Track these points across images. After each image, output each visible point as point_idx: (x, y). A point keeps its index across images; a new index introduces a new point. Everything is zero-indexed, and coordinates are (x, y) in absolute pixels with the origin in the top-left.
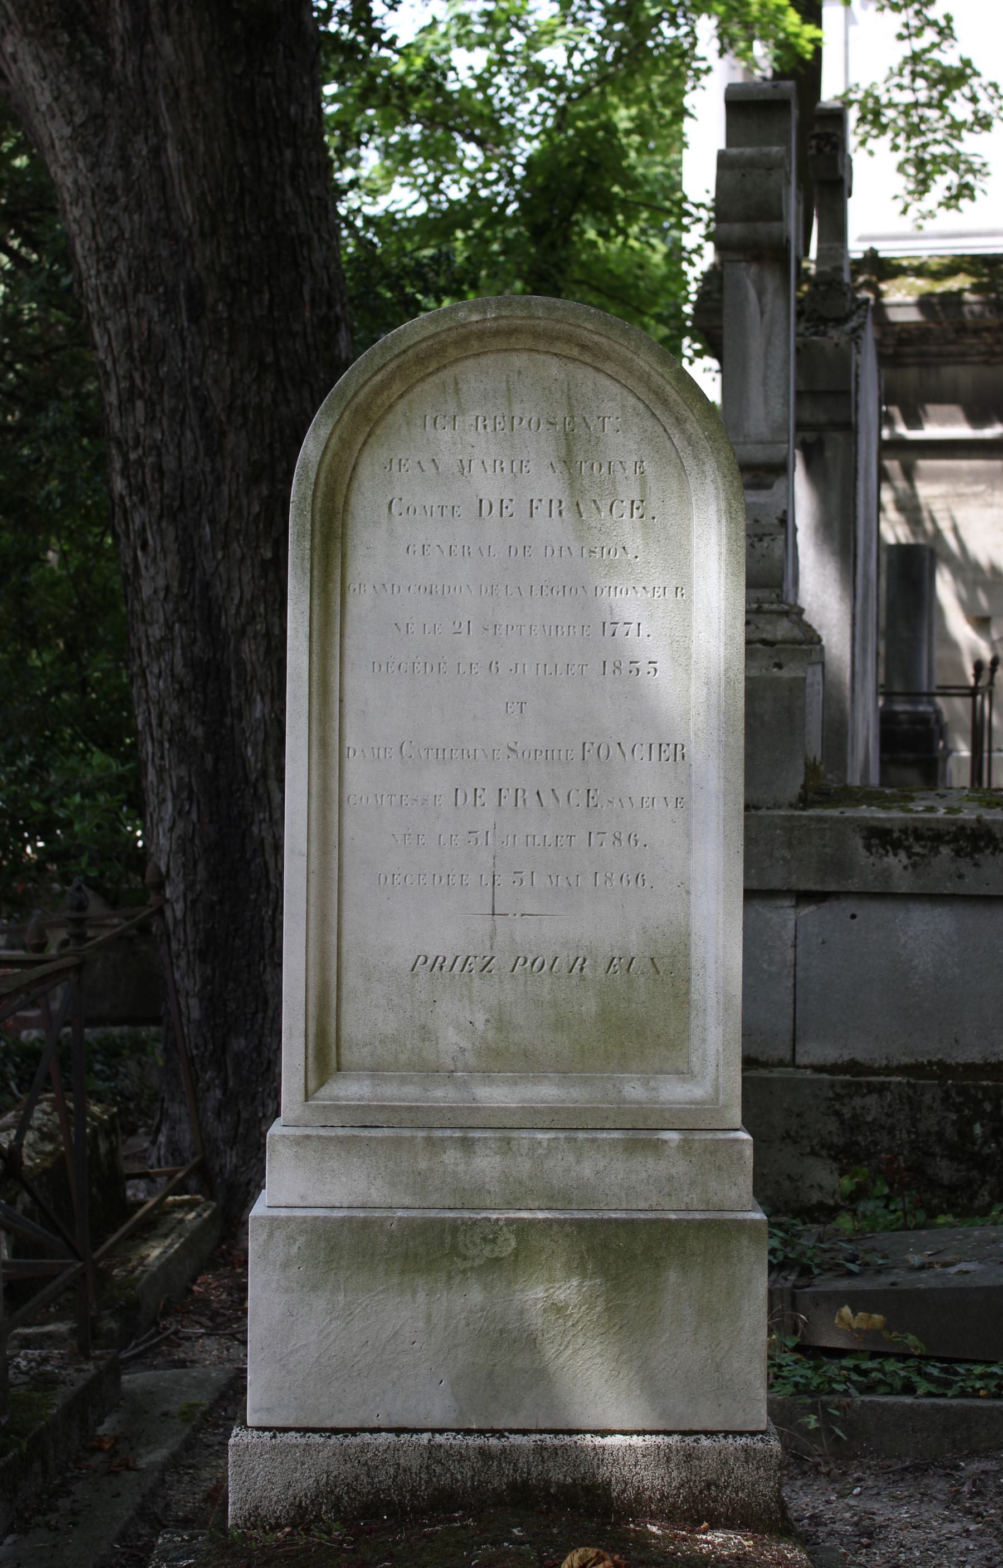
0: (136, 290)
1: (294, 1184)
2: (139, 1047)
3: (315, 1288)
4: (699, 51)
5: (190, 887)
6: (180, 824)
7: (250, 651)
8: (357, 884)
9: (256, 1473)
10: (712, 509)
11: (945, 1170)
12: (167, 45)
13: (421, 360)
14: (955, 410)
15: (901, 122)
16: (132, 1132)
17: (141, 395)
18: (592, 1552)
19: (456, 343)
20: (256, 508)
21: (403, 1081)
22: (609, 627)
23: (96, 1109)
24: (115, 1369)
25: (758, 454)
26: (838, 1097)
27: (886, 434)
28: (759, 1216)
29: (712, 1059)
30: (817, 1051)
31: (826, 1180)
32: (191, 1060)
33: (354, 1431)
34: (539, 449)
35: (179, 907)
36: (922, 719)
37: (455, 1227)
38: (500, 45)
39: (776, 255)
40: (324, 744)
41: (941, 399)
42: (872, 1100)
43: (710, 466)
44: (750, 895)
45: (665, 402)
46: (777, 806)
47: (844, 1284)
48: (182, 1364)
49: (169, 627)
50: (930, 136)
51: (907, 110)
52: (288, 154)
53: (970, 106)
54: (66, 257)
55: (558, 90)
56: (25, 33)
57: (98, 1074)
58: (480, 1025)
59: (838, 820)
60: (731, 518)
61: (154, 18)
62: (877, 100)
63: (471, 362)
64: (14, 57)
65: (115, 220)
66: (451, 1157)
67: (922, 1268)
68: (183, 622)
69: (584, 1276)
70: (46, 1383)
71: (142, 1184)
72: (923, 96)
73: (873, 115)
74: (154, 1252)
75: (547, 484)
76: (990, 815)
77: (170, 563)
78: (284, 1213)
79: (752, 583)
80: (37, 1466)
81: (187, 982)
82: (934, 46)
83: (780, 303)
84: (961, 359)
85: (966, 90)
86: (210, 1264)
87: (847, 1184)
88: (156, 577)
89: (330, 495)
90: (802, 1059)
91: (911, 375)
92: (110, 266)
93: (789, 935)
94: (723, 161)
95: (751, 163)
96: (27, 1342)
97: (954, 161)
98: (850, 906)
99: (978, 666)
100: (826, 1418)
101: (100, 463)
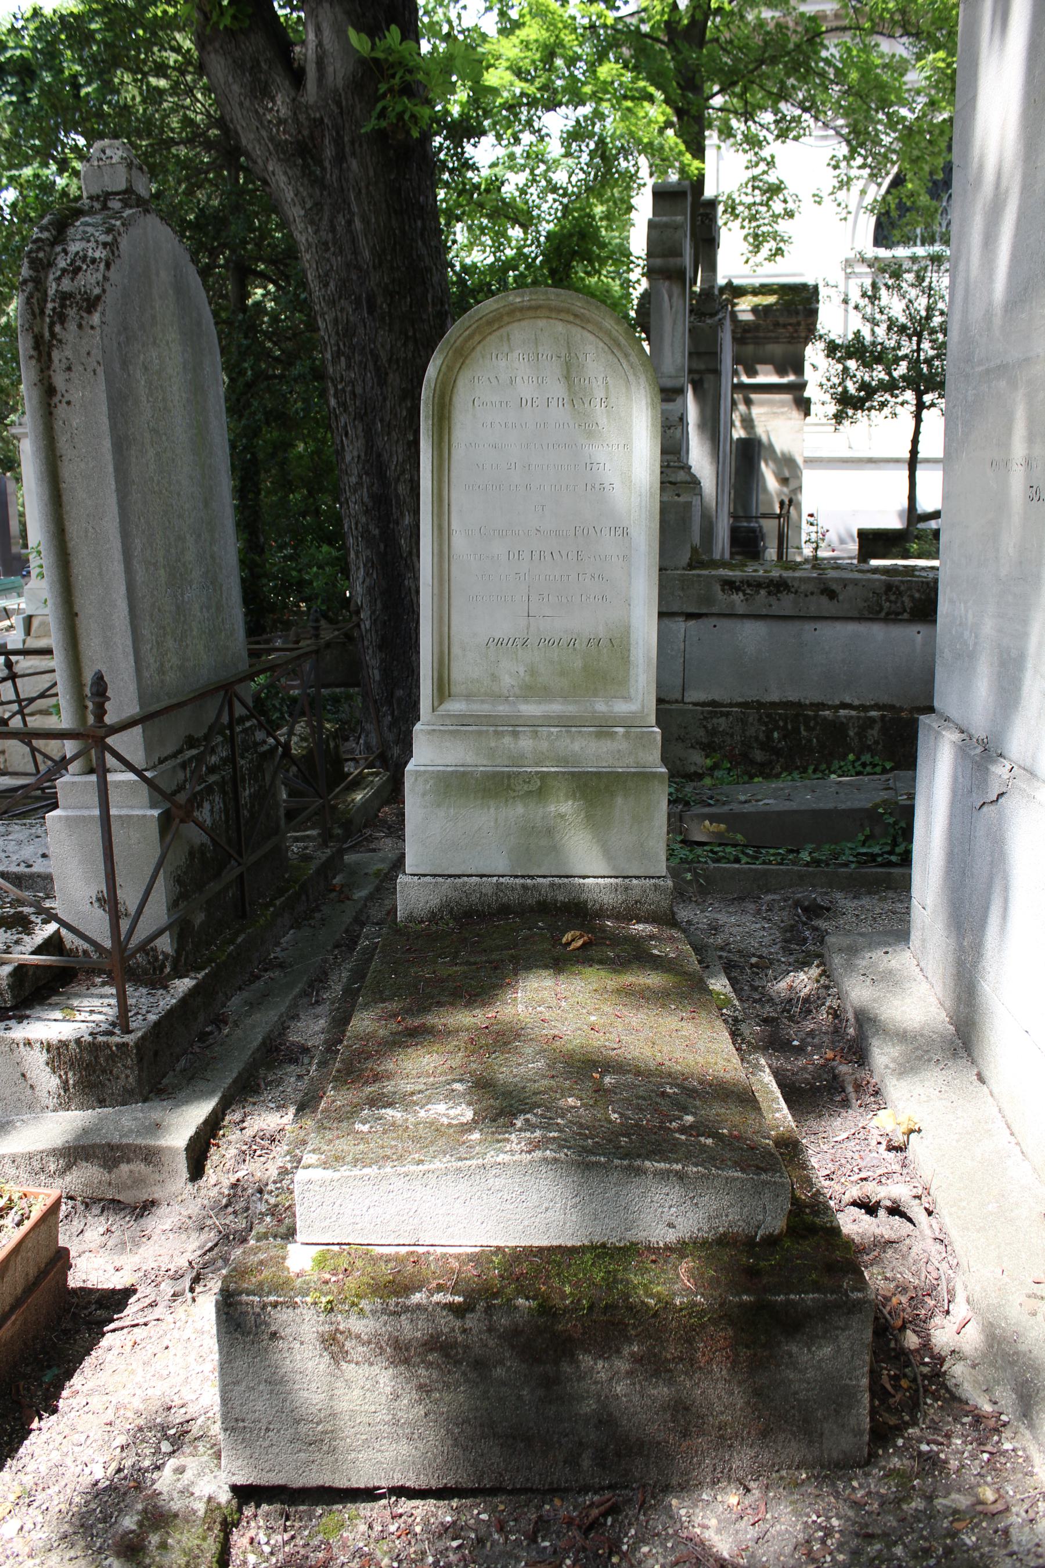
0: (340, 298)
1: (428, 753)
2: (349, 697)
3: (439, 806)
4: (639, 175)
5: (373, 612)
6: (368, 580)
7: (402, 489)
8: (458, 601)
9: (412, 897)
10: (644, 402)
11: (759, 756)
12: (354, 164)
13: (489, 323)
14: (770, 367)
15: (746, 213)
16: (347, 739)
17: (343, 354)
18: (578, 933)
19: (509, 314)
20: (404, 413)
21: (483, 702)
22: (590, 466)
23: (328, 726)
24: (341, 852)
25: (669, 383)
26: (705, 718)
27: (735, 380)
28: (664, 770)
29: (641, 691)
30: (695, 695)
31: (698, 760)
32: (376, 701)
33: (459, 876)
34: (553, 369)
35: (368, 623)
36: (753, 530)
37: (509, 775)
38: (532, 171)
39: (677, 276)
40: (440, 528)
41: (764, 362)
42: (722, 720)
43: (643, 380)
44: (661, 615)
45: (619, 345)
46: (676, 569)
47: (706, 810)
48: (374, 850)
49: (361, 477)
50: (761, 222)
51: (749, 207)
52: (419, 223)
53: (783, 205)
54: (303, 284)
55: (565, 195)
56: (279, 159)
57: (329, 711)
58: (522, 674)
59: (708, 576)
60: (654, 407)
61: (347, 149)
62: (733, 201)
63: (516, 324)
64: (273, 173)
65: (328, 260)
66: (507, 740)
67: (746, 802)
68: (367, 474)
69: (575, 799)
70: (306, 858)
71: (351, 764)
72: (758, 200)
73: (732, 209)
74: (359, 797)
75: (557, 389)
76: (786, 574)
77: (360, 443)
78: (422, 768)
79: (664, 452)
80: (304, 898)
81: (372, 661)
82: (765, 172)
83: (681, 302)
84: (776, 340)
85: (781, 196)
86: (387, 802)
87: (709, 762)
88: (353, 450)
89: (442, 396)
90: (687, 700)
91: (750, 349)
92: (326, 285)
93: (681, 636)
94: (651, 224)
95: (666, 225)
96: (297, 839)
97: (775, 236)
98: (713, 621)
99: (782, 503)
100: (696, 875)
101: (323, 394)
